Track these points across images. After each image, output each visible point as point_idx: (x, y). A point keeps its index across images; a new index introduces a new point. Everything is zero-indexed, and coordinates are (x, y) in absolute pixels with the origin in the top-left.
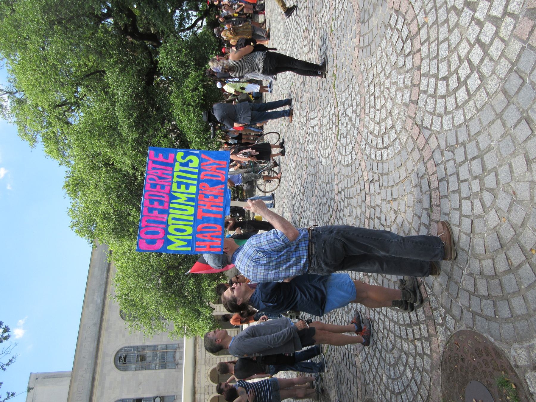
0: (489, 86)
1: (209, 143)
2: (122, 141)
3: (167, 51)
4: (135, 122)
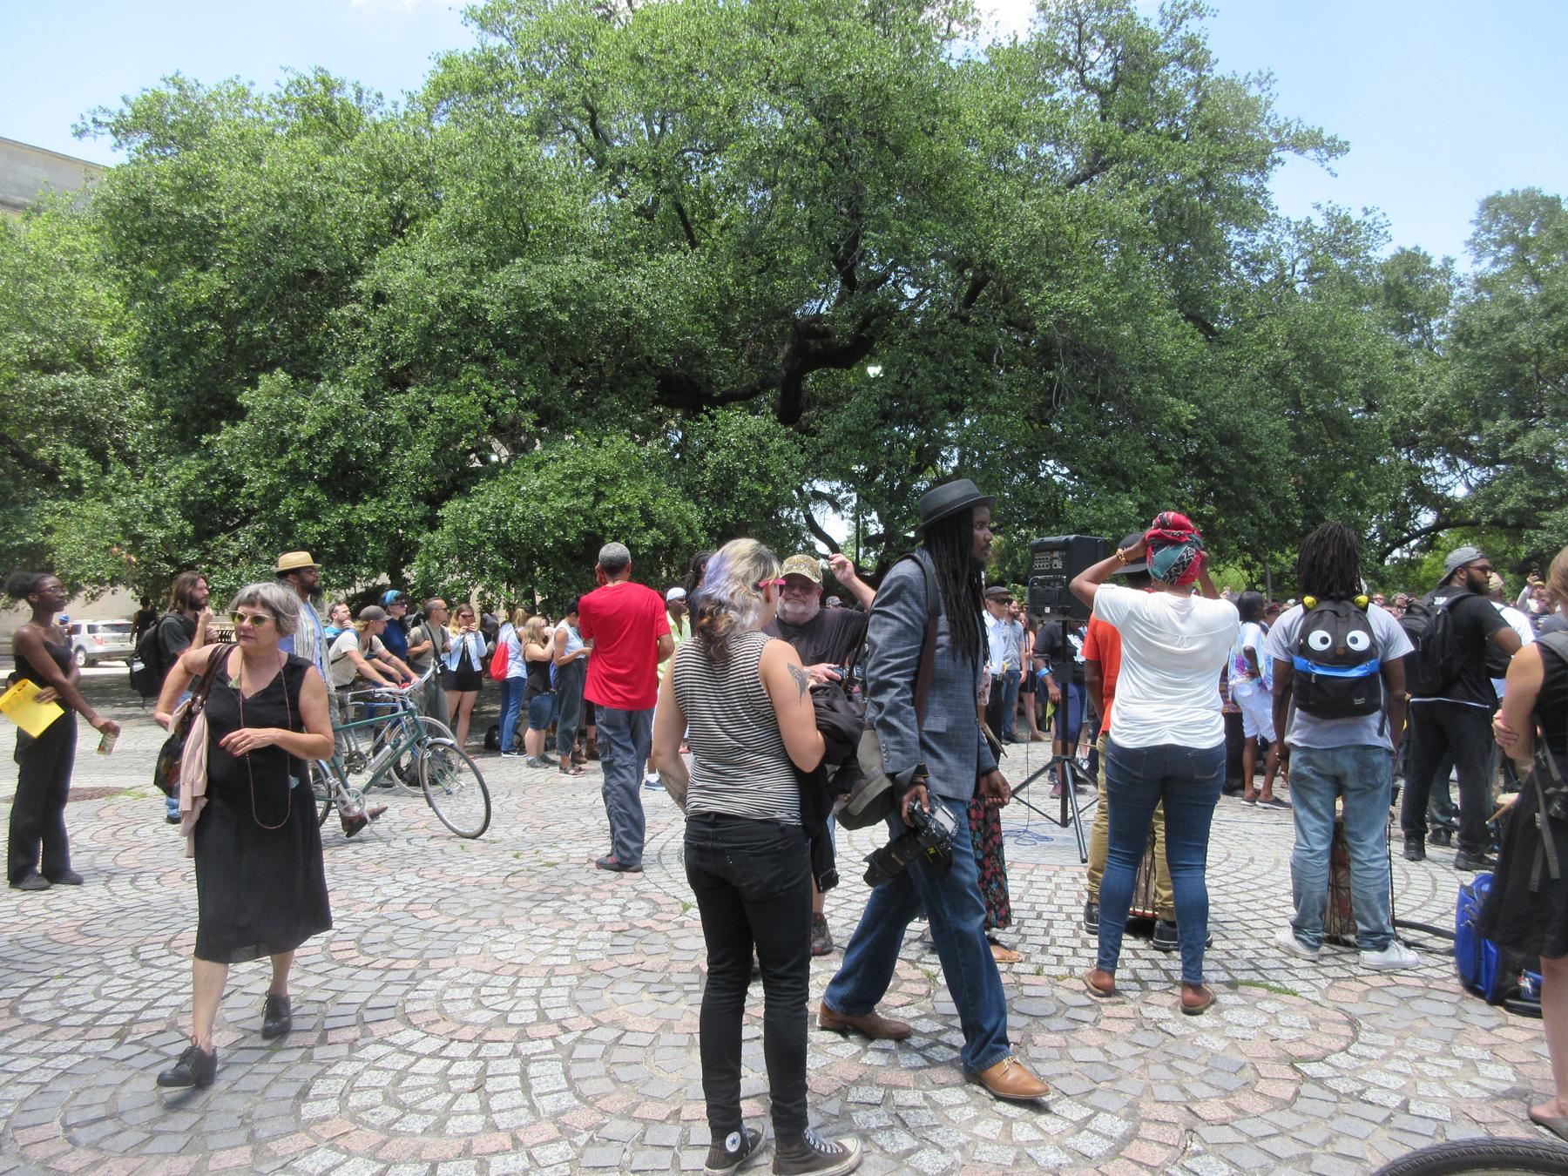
0: (720, 374)
1: (462, 559)
2: (474, 267)
3: (765, 439)
4: (540, 314)
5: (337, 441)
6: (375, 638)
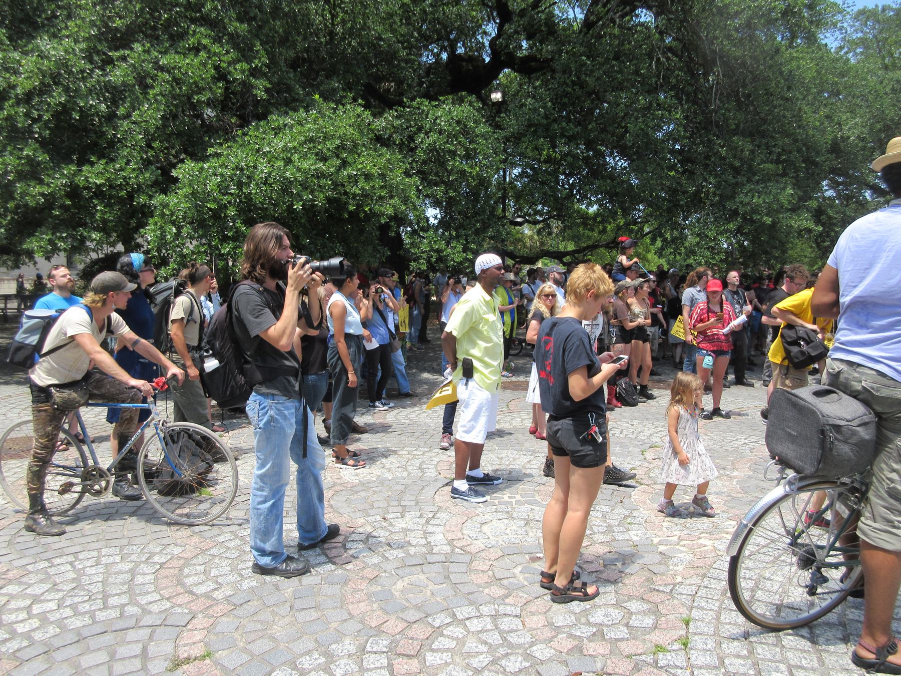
5: (58, 97)
6: (115, 316)
